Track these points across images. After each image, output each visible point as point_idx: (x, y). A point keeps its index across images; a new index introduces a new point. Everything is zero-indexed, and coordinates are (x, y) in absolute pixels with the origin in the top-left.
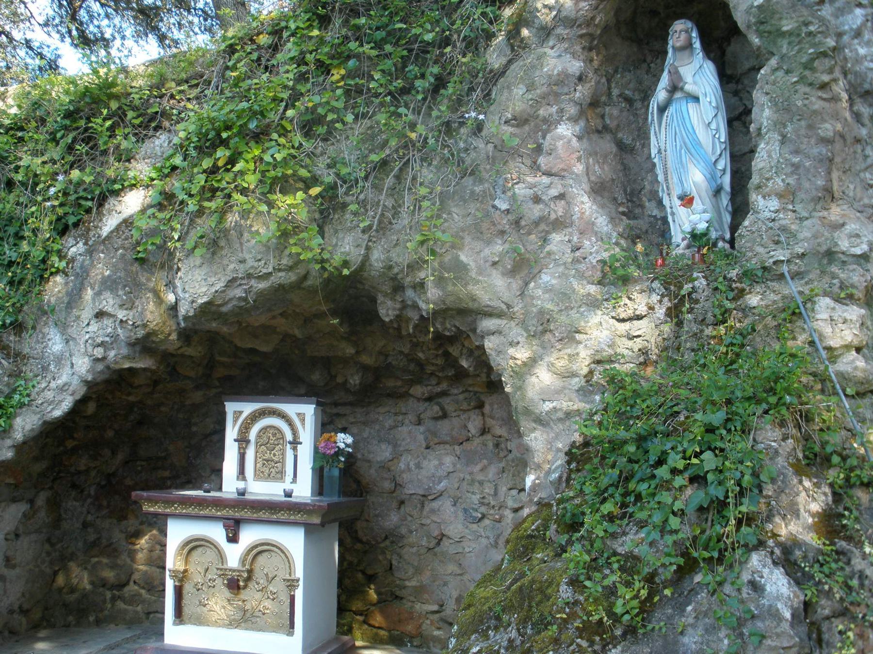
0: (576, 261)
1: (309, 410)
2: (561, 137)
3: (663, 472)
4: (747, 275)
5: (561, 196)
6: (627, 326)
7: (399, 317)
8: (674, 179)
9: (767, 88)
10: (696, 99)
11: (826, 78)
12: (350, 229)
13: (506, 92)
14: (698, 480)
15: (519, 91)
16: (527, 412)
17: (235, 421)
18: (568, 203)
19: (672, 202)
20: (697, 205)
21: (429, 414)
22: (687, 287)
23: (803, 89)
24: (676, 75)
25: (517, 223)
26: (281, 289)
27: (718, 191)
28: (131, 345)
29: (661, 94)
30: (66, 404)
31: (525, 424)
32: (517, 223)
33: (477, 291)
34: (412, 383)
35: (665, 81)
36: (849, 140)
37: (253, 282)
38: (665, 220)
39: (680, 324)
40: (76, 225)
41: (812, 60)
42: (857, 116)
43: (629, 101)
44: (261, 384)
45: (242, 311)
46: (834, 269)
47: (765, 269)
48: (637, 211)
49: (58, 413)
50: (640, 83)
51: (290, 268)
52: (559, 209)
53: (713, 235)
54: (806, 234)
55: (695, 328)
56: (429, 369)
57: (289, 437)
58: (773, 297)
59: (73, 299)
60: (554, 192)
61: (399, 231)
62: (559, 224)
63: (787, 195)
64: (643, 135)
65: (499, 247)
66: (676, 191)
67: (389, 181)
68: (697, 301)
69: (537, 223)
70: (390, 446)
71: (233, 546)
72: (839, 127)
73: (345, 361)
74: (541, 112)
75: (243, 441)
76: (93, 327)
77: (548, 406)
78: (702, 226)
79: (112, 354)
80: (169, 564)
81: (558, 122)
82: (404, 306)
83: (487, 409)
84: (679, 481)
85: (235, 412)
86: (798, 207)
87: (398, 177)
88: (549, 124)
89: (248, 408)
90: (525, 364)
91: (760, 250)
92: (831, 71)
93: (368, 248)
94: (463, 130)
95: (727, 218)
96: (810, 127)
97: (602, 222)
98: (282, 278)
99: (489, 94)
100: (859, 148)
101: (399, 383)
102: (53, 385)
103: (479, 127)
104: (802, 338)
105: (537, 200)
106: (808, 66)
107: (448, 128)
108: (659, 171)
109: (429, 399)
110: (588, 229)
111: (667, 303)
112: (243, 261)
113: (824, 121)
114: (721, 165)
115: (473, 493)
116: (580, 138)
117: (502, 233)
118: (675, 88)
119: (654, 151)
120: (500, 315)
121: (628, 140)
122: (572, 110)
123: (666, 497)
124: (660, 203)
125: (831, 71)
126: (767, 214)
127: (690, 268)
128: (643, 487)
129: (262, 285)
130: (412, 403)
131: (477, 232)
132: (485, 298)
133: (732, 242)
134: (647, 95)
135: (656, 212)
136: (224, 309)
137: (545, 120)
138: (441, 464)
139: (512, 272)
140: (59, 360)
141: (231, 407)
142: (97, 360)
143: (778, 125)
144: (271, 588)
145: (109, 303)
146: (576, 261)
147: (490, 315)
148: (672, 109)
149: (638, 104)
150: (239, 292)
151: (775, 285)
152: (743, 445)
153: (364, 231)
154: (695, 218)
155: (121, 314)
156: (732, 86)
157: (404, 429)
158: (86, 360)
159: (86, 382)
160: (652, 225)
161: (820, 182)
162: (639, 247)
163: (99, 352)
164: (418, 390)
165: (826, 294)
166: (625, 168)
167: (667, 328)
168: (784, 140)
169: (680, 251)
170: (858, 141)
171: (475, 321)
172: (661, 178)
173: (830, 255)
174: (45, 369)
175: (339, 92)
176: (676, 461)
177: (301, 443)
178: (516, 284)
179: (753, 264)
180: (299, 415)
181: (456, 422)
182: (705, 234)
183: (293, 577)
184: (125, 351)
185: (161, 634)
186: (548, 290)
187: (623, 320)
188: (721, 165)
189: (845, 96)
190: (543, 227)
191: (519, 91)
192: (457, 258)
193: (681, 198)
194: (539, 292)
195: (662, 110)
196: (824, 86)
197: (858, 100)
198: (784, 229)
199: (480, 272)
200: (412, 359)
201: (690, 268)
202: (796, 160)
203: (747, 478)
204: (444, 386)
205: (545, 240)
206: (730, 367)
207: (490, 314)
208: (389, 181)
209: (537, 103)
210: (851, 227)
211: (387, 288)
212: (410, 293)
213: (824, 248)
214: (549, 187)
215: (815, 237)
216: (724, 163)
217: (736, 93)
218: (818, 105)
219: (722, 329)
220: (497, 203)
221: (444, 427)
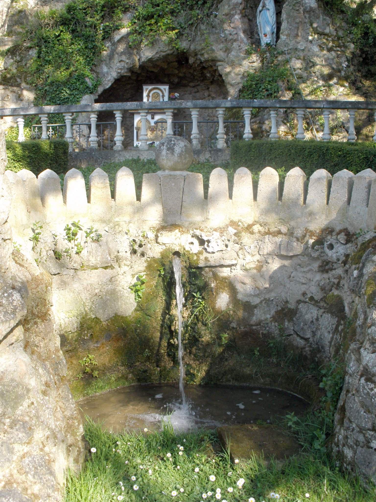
0: (239, 49)
1: (167, 87)
2: (236, 19)
3: (260, 89)
4: (278, 53)
5: (236, 34)
6: (251, 64)
7: (194, 63)
8: (262, 30)
9: (285, 9)
10: (269, 10)
11: (298, 8)
12: (185, 40)
13: (223, 7)
14: (267, 90)
15: (226, 7)
16: (229, 83)
18: (238, 35)
19: (262, 35)
20: (268, 36)
21: (194, 91)
22: (265, 55)
23: (293, 11)
24: (264, 3)
25: (226, 40)
26: (168, 55)
27: (273, 33)
28: (127, 69)
29: (260, 8)
30: (110, 84)
31: (228, 86)
32: (226, 40)
33: (217, 55)
34: (190, 82)
35: (261, 4)
36: (303, 22)
37: (162, 53)
38: (260, 39)
39: (263, 64)
40: (108, 38)
41: (295, 4)
42: (305, 17)
43: (252, 8)
44: (149, 82)
45: (159, 60)
46: (297, 52)
47: (282, 52)
48: (253, 37)
49: (107, 87)
50: (255, 2)
51: (171, 50)
52: (236, 37)
53: (272, 44)
54: (292, 44)
55: (267, 64)
56: (196, 77)
57: (161, 94)
58: (284, 58)
59: (111, 57)
60: (235, 33)
61: (198, 41)
62: (235, 40)
63: (288, 35)
64: (255, 17)
65: (222, 45)
66: (263, 33)
67: (194, 28)
68: (267, 59)
69: (231, 40)
72: (300, 20)
73: (174, 75)
74: (231, 12)
75: (148, 96)
76: (118, 64)
77: (234, 82)
78: (269, 42)
79: (123, 71)
81: (235, 15)
82: (197, 59)
83: (210, 89)
84: (263, 90)
86: (290, 38)
87: (196, 28)
88: (234, 15)
89: (150, 87)
90: (228, 72)
91: (282, 47)
92: (299, 7)
93: (190, 45)
94: (211, 16)
95: (275, 40)
96: (294, 20)
97: (245, 40)
98: (169, 52)
99: (217, 6)
100: (305, 24)
101: (187, 82)
102: (107, 79)
103: (216, 16)
104: (289, 66)
105: (231, 34)
106: (294, 5)
107: (208, 16)
108: (259, 27)
109: (194, 87)
110: (242, 41)
111: (261, 59)
112: (159, 48)
113: (297, 18)
114: (274, 27)
115: (206, 113)
116: (240, 19)
117: (223, 42)
118: (263, 7)
119: (258, 22)
120: (222, 61)
121: (251, 18)
122: (239, 12)
123: (261, 93)
124: (259, 35)
125: (299, 7)
126: (284, 40)
127: (266, 51)
128: (257, 93)
129: (164, 54)
130: (189, 88)
131: (217, 41)
132: (219, 58)
133: (276, 45)
134: (256, 6)
135: (257, 37)
136: (154, 60)
137: (232, 15)
139: (225, 51)
140: (107, 73)
141: (145, 87)
142: (119, 73)
143: (287, 19)
145: (124, 58)
146: (239, 49)
147: (220, 61)
148: (263, 12)
149: (254, 8)
150: (158, 56)
151: (284, 55)
152: (275, 84)
153: (189, 41)
154: (267, 40)
155: (127, 61)
156: (278, 4)
157: (186, 96)
158: (116, 73)
159: (115, 79)
160: (256, 41)
161: (295, 33)
162: (254, 46)
163: (119, 71)
164: (192, 84)
165: (295, 57)
166: (250, 26)
167: (260, 65)
168: (288, 22)
169: (264, 47)
170: (305, 23)
171: (216, 63)
172: (259, 29)
173: (296, 49)
174: (104, 75)
175: (179, 4)
176: (263, 87)
178: (226, 54)
179: (280, 51)
181: (201, 93)
182: (270, 43)
184: (126, 71)
186: (233, 56)
187: (250, 63)
188: (274, 27)
189: (302, 12)
190: (232, 41)
191: (226, 7)
192: (212, 48)
193: (264, 34)
194: (231, 56)
195: (260, 12)
196: (297, 10)
197: (306, 13)
198: (287, 43)
199: (218, 51)
200: (192, 75)
201: (266, 51)
202: (290, 27)
203: (276, 89)
204: (199, 83)
205: (232, 44)
206: (274, 71)
207: (220, 61)
208: (194, 28)
209: (231, 10)
210: (301, 43)
211: (193, 55)
212: (199, 56)
213: (295, 48)
214: (233, 31)
215: (294, 45)
216: (275, 26)
217: (279, 6)
218: (296, 15)
219: (273, 64)
220: (221, 35)
221: (198, 95)
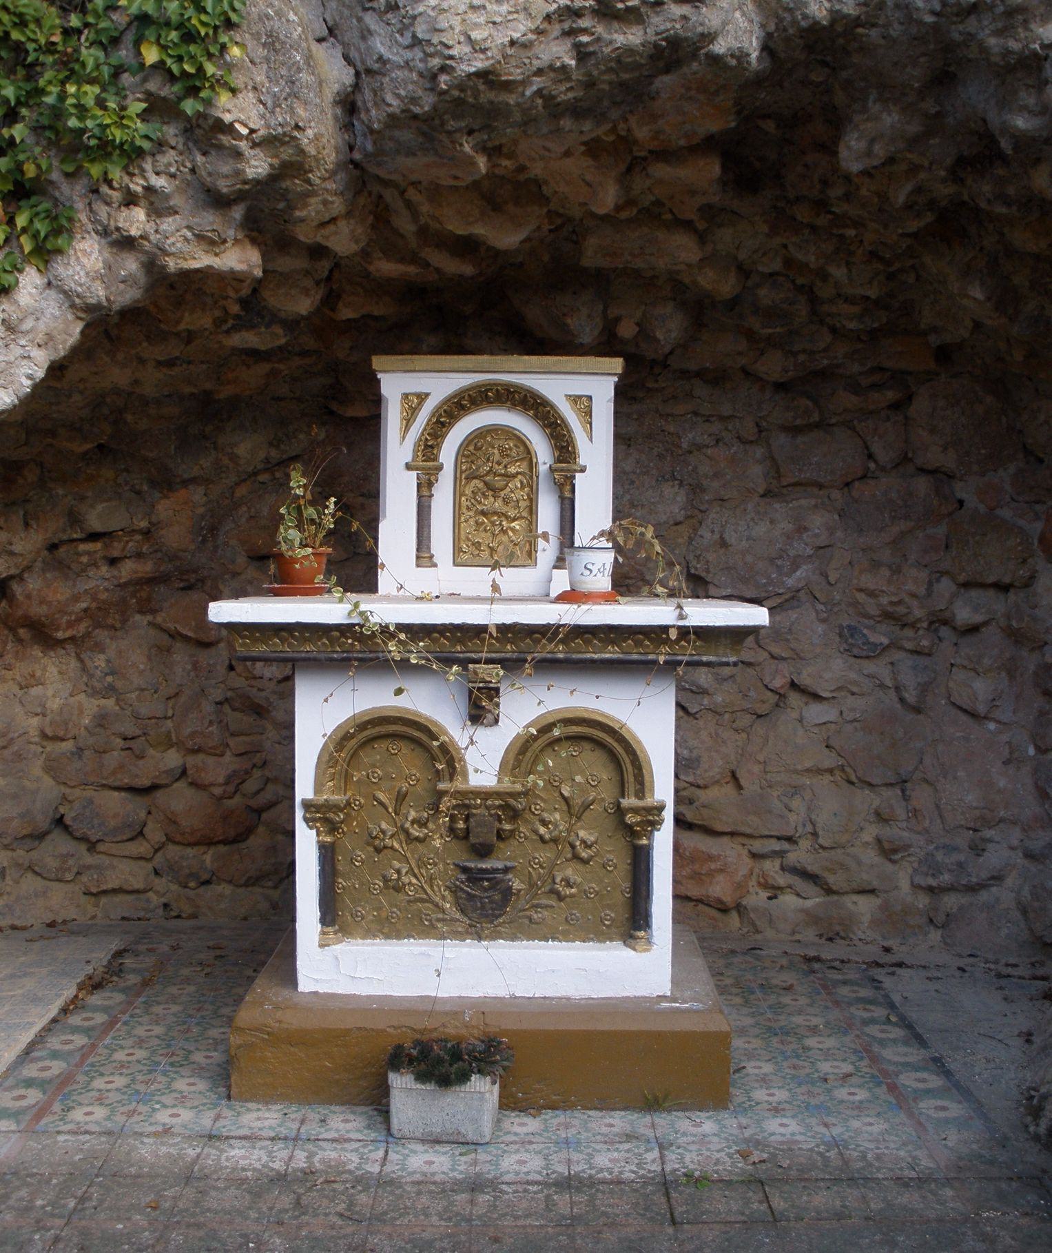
17: (408, 422)
70: (682, 492)
71: (483, 734)
80: (304, 788)
85: (406, 396)
138: (801, 529)
144: (582, 833)
177: (583, 470)
180: (575, 399)
183: (648, 802)
185: (289, 976)
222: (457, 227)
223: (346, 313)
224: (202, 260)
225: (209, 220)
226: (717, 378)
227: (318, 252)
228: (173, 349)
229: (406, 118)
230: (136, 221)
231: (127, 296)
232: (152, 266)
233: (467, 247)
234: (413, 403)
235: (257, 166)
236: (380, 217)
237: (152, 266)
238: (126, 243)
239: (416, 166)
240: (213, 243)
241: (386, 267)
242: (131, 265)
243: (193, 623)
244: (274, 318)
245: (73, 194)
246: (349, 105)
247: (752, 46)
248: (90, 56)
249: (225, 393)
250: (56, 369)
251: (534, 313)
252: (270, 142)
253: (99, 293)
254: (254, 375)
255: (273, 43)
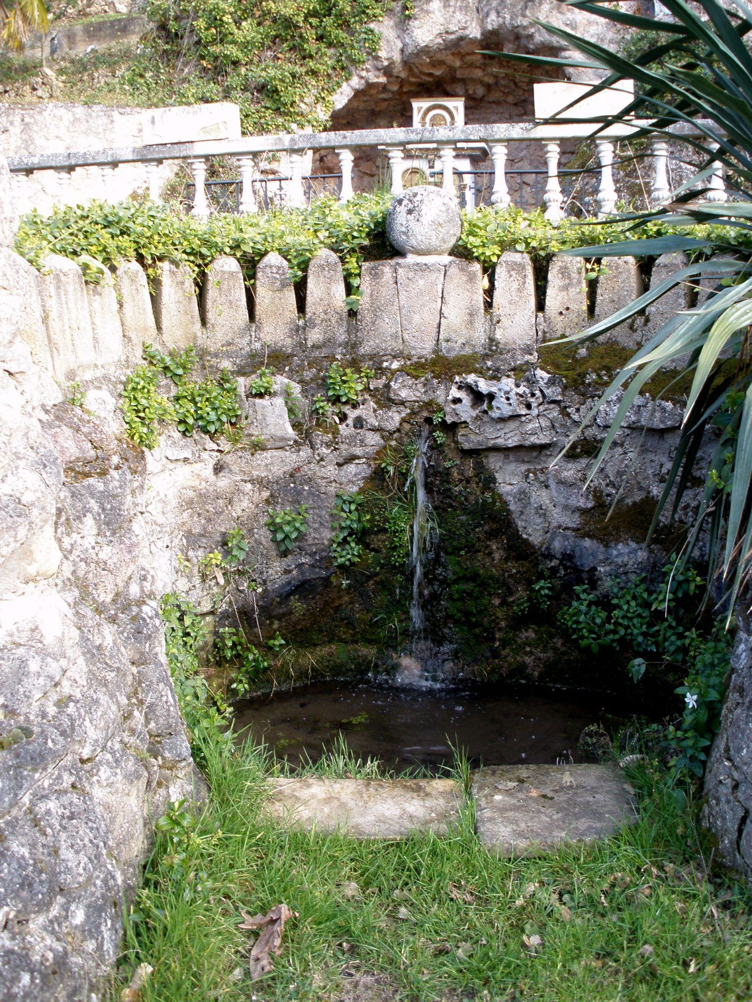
222: (427, 71)
223: (405, 90)
224: (376, 80)
225: (377, 73)
226: (498, 103)
227: (398, 77)
228: (367, 98)
229: (412, 53)
230: (364, 74)
231: (362, 87)
232: (367, 82)
233: (431, 75)
234: (419, 109)
235: (386, 63)
236: (411, 70)
237: (367, 82)
238: (362, 78)
239: (416, 61)
240: (378, 77)
241: (413, 80)
242: (363, 81)
243: (260, 590)
244: (389, 91)
245: (353, 69)
246: (402, 51)
247: (479, 36)
248: (356, 45)
249: (377, 109)
250: (349, 101)
251: (449, 88)
252: (388, 59)
253: (357, 87)
254: (384, 105)
255: (388, 41)
